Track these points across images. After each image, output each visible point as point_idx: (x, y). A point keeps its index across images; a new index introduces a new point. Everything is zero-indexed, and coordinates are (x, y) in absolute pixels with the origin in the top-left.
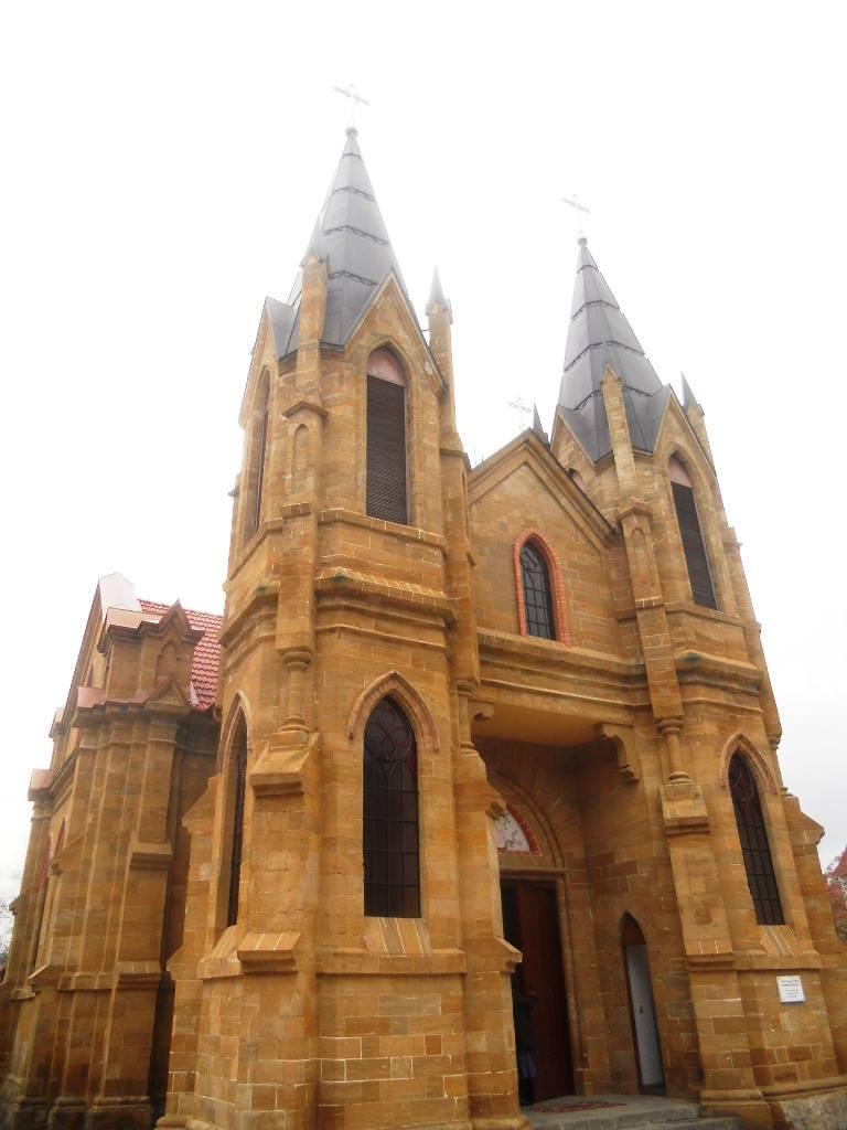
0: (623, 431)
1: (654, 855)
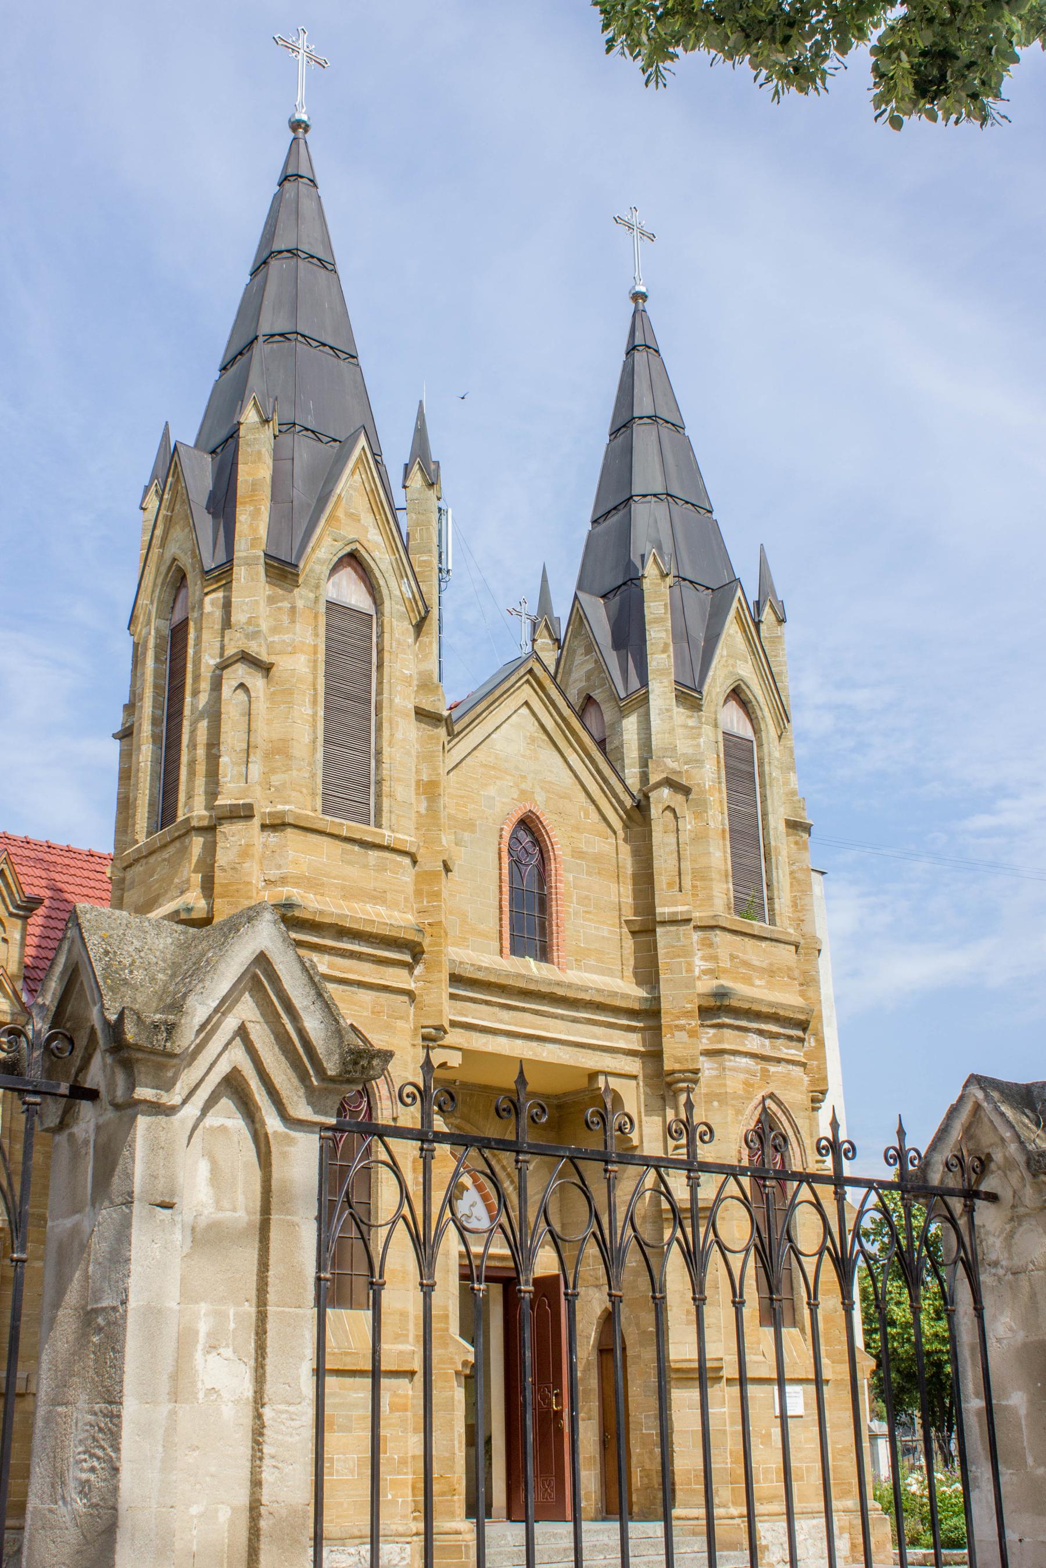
0: (664, 656)
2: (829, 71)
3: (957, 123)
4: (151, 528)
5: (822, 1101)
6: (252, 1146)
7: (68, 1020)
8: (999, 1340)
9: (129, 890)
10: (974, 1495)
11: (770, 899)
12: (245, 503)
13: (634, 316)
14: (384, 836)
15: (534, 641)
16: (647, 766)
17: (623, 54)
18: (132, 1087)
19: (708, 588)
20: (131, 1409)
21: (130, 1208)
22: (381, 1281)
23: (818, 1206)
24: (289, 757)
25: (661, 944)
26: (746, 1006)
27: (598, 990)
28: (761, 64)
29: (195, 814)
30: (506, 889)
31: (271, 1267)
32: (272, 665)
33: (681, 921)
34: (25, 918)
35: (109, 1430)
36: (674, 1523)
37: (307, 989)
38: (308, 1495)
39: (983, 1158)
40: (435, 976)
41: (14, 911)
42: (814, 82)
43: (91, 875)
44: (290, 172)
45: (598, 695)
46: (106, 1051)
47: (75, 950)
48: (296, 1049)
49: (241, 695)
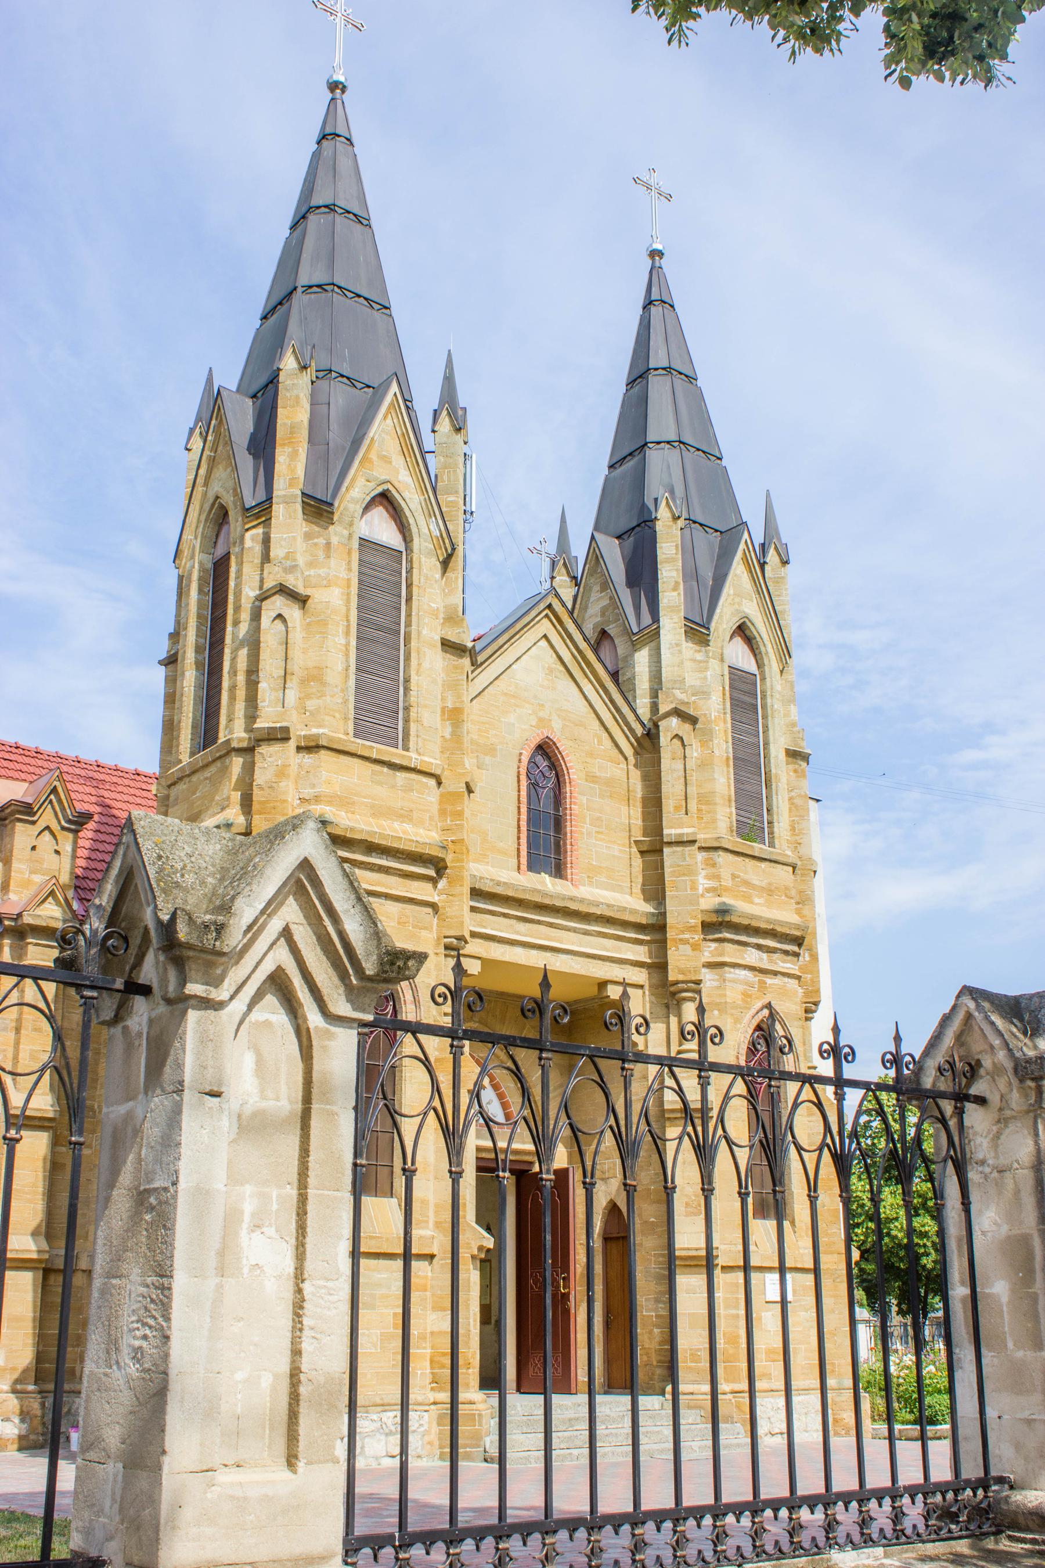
0: (675, 594)
1: (145, 1474)
2: (844, 32)
3: (962, 83)
4: (195, 467)
5: (815, 1011)
6: (295, 1040)
7: (123, 920)
8: (983, 1233)
9: (174, 806)
10: (958, 1375)
11: (770, 823)
12: (284, 445)
13: (651, 272)
14: (411, 758)
15: (552, 578)
16: (657, 697)
17: (648, 13)
18: (183, 982)
19: (716, 531)
20: (181, 1282)
21: (180, 1096)
22: (413, 1168)
23: (819, 1105)
24: (324, 684)
25: (667, 863)
26: (746, 922)
27: (608, 906)
28: (779, 24)
29: (235, 736)
30: (524, 809)
31: (311, 1153)
32: (308, 597)
33: (687, 842)
34: (76, 832)
35: (161, 1301)
36: (681, 1397)
37: (348, 893)
38: (345, 1366)
39: (973, 1063)
40: (457, 890)
41: (66, 825)
42: (830, 43)
43: (138, 792)
44: (328, 131)
45: (612, 630)
46: (159, 949)
47: (130, 854)
48: (337, 950)
49: (279, 625)
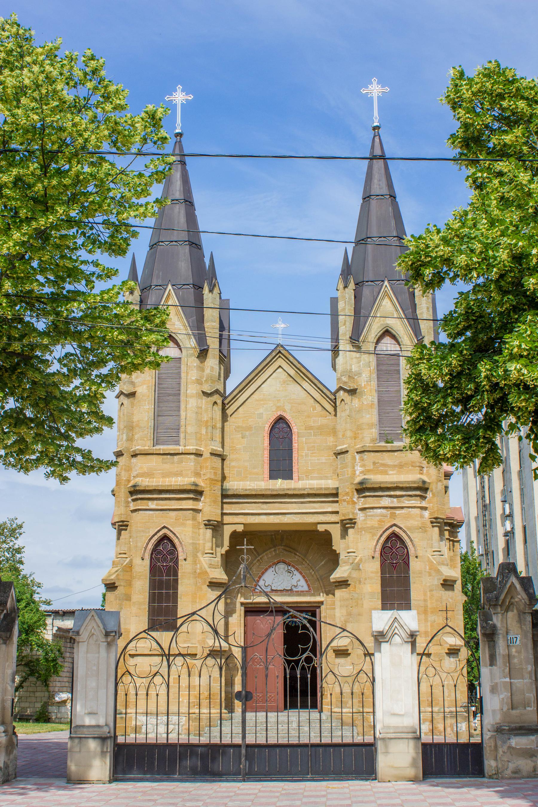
26: (377, 486)
27: (311, 489)
